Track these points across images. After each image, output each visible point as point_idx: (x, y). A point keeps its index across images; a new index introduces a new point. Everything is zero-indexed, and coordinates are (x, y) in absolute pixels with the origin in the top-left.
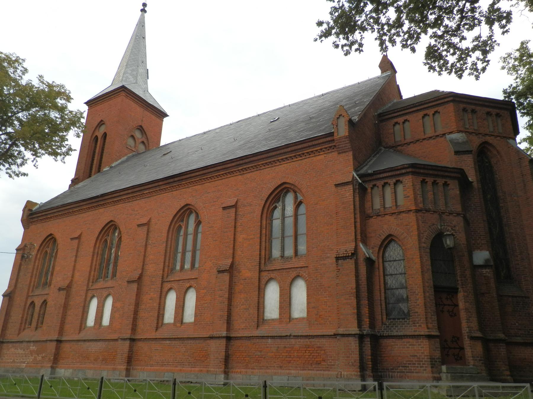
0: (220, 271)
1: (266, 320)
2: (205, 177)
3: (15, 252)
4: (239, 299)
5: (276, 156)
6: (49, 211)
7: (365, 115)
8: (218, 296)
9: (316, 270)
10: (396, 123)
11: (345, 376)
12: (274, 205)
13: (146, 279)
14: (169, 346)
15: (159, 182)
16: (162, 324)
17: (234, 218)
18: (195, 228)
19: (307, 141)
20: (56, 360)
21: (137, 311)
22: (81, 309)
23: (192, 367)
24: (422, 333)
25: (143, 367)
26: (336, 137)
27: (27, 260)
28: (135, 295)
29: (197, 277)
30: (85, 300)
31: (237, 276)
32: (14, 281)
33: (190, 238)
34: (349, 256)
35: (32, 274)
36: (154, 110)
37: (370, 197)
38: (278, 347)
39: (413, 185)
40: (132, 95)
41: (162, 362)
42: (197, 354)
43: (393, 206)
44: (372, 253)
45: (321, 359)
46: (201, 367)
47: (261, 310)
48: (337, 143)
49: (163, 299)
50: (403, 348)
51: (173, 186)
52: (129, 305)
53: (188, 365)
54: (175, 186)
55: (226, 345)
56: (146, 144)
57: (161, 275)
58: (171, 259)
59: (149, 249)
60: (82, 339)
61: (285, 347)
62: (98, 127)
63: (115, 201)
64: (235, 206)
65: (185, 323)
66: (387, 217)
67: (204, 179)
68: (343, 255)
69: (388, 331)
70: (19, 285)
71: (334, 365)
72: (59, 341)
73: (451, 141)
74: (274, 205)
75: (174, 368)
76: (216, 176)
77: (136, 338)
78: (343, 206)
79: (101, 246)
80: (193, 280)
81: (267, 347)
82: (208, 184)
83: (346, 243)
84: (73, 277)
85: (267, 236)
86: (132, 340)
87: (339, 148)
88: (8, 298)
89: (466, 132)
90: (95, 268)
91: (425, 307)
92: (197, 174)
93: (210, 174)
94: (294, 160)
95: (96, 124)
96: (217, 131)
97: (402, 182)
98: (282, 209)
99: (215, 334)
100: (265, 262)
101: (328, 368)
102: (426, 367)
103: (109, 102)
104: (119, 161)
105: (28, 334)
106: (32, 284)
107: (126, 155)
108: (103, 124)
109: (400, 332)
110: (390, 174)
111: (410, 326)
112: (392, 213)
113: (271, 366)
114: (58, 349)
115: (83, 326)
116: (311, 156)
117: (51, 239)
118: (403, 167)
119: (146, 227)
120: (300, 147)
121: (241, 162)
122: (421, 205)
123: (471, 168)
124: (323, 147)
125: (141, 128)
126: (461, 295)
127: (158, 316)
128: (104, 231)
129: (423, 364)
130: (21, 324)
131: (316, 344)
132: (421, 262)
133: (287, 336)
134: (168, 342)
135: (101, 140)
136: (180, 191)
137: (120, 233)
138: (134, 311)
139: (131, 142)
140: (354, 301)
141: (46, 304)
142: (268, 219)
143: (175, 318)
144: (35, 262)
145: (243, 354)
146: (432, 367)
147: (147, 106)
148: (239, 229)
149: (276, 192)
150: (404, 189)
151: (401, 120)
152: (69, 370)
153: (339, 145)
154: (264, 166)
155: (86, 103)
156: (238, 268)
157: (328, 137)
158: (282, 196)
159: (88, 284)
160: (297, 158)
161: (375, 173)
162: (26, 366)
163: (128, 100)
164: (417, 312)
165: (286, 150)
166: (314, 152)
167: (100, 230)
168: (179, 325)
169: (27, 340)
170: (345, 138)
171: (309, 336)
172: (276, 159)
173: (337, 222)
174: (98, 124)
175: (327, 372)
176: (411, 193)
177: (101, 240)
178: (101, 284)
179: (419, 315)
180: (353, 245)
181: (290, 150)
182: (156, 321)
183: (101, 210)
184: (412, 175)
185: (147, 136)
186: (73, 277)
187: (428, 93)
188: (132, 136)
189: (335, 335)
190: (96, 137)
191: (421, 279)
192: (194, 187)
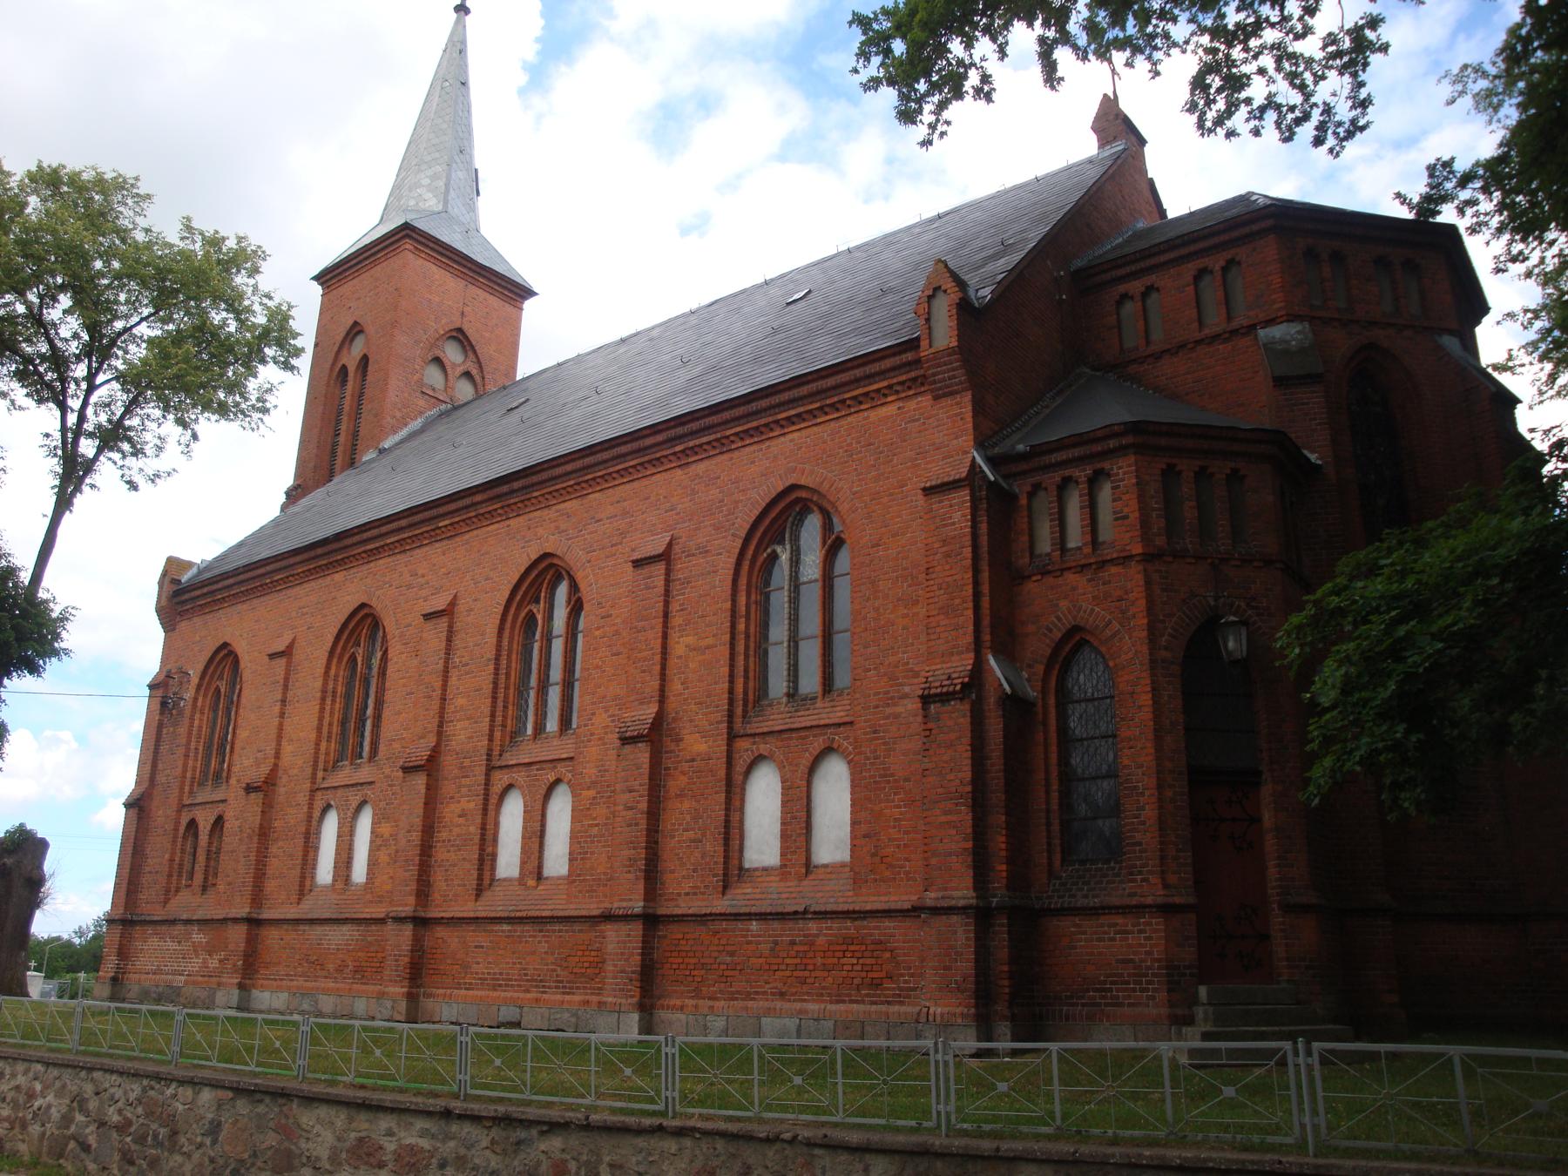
0: (626, 738)
1: (748, 870)
2: (590, 477)
3: (147, 692)
4: (678, 813)
5: (772, 411)
6: (217, 582)
7: (1016, 283)
8: (621, 807)
9: (875, 732)
10: (1125, 297)
11: (938, 1019)
12: (769, 550)
13: (448, 762)
14: (508, 937)
15: (473, 494)
16: (493, 880)
17: (661, 590)
18: (569, 618)
19: (849, 365)
20: (250, 967)
21: (431, 847)
22: (300, 841)
23: (564, 993)
24: (1149, 900)
25: (449, 991)
26: (925, 351)
27: (174, 712)
28: (422, 805)
29: (572, 755)
30: (310, 817)
31: (671, 752)
32: (148, 767)
33: (558, 646)
34: (954, 692)
35: (188, 749)
36: (495, 282)
37: (1026, 520)
38: (776, 943)
39: (1138, 484)
40: (431, 245)
41: (493, 979)
42: (577, 959)
43: (1085, 544)
44: (1028, 680)
45: (883, 974)
46: (586, 994)
47: (735, 843)
48: (929, 368)
49: (491, 813)
50: (1099, 940)
51: (509, 506)
52: (409, 831)
53: (556, 987)
54: (515, 503)
55: (644, 936)
56: (478, 378)
57: (484, 751)
58: (510, 707)
59: (453, 681)
60: (304, 917)
61: (793, 943)
62: (346, 346)
63: (371, 550)
64: (666, 557)
65: (547, 878)
66: (1070, 577)
67: (587, 481)
68: (939, 690)
69: (1063, 897)
70: (161, 778)
71: (914, 989)
72: (254, 922)
73: (1269, 347)
74: (769, 550)
75: (521, 995)
76: (618, 472)
77: (430, 915)
78: (944, 549)
79: (342, 673)
80: (563, 764)
81: (749, 943)
82: (597, 495)
83: (952, 654)
84: (277, 755)
85: (752, 639)
86: (421, 923)
87: (935, 382)
88: (136, 810)
89: (1314, 318)
90: (330, 733)
91: (1160, 829)
92: (569, 467)
93: (601, 467)
94: (819, 420)
95: (343, 334)
96: (655, 333)
97: (1109, 475)
98: (791, 559)
99: (617, 906)
100: (745, 712)
101: (900, 996)
102: (1155, 990)
103: (372, 271)
104: (404, 433)
105: (186, 903)
106: (189, 775)
107: (421, 413)
108: (361, 331)
109: (1094, 897)
110: (1077, 452)
111: (1120, 882)
112: (1083, 566)
113: (757, 993)
114: (252, 941)
115: (308, 883)
116: (862, 407)
117: (225, 659)
118: (1110, 432)
119: (445, 619)
120: (831, 382)
121: (680, 430)
122: (1160, 541)
123: (1320, 424)
124: (895, 381)
125: (459, 336)
126: (1267, 791)
127: (481, 860)
128: (345, 637)
129: (1149, 983)
130: (170, 875)
131: (871, 935)
132: (1155, 702)
133: (796, 913)
134: (505, 927)
135: (355, 377)
136: (526, 517)
137: (574, 587)
138: (422, 845)
139: (434, 376)
140: (965, 816)
141: (222, 827)
142: (753, 590)
143: (523, 863)
144: (192, 719)
145: (687, 960)
146: (1169, 991)
147: (474, 271)
148: (677, 620)
149: (772, 515)
150: (1113, 494)
151: (1136, 287)
152: (280, 995)
153: (934, 375)
154: (742, 439)
155: (317, 278)
156: (674, 729)
157: (905, 351)
158: (789, 525)
159: (314, 775)
160: (826, 414)
161: (1036, 452)
162: (186, 982)
163: (420, 262)
164: (1140, 844)
165: (795, 393)
166: (872, 395)
167: (336, 631)
168: (531, 883)
169: (184, 917)
170: (949, 355)
171: (854, 912)
172: (771, 419)
173: (928, 595)
174: (348, 334)
175: (896, 1008)
176: (1132, 509)
177: (207, 689)
178: (345, 775)
179: (1145, 851)
180: (965, 662)
181: (805, 393)
182: (475, 874)
183: (338, 577)
184: (1135, 453)
185: (477, 357)
186: (277, 755)
187: (1227, 202)
188: (438, 361)
189: (915, 911)
190: (344, 368)
191: (1153, 751)
192: (562, 506)
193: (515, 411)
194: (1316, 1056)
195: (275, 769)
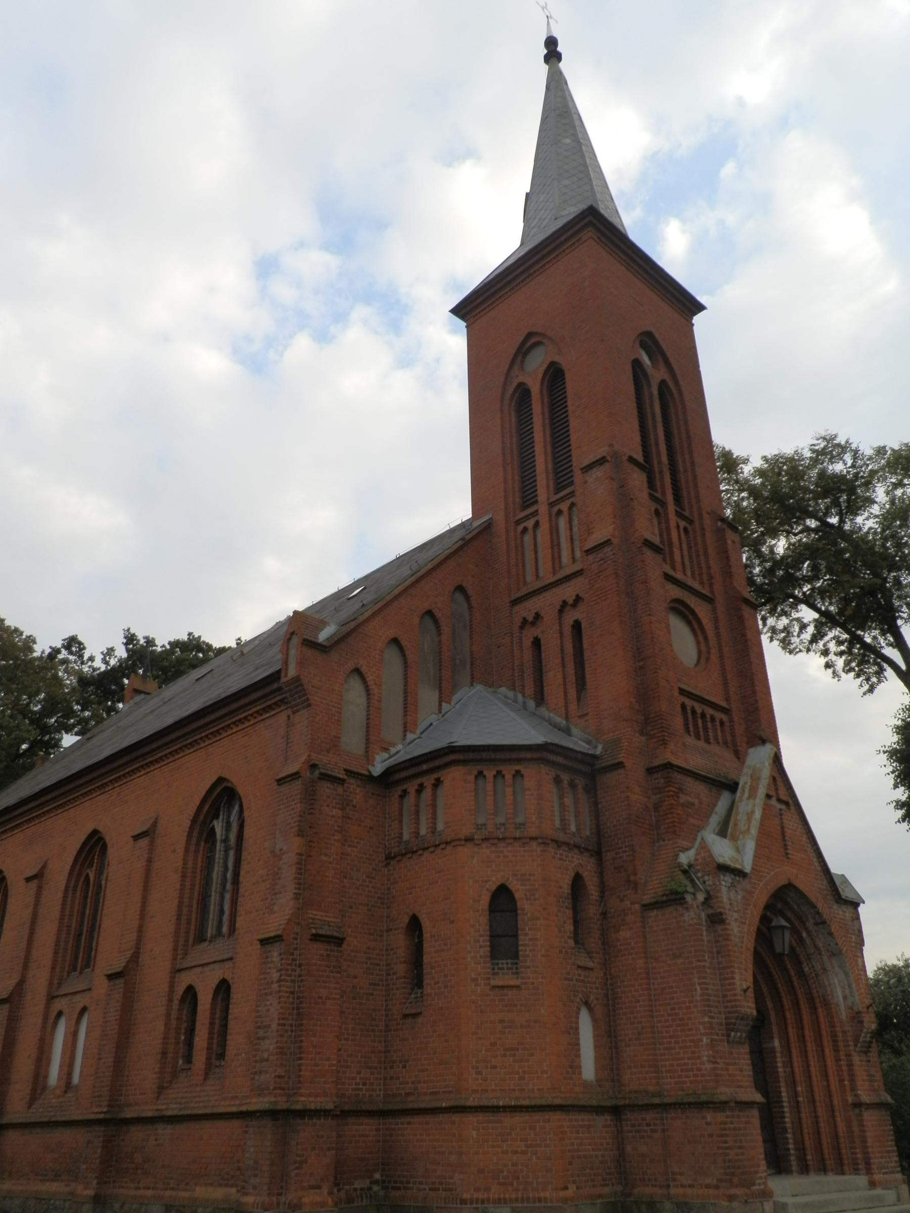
190: (523, 393)
193: (203, 680)
195: (135, 957)
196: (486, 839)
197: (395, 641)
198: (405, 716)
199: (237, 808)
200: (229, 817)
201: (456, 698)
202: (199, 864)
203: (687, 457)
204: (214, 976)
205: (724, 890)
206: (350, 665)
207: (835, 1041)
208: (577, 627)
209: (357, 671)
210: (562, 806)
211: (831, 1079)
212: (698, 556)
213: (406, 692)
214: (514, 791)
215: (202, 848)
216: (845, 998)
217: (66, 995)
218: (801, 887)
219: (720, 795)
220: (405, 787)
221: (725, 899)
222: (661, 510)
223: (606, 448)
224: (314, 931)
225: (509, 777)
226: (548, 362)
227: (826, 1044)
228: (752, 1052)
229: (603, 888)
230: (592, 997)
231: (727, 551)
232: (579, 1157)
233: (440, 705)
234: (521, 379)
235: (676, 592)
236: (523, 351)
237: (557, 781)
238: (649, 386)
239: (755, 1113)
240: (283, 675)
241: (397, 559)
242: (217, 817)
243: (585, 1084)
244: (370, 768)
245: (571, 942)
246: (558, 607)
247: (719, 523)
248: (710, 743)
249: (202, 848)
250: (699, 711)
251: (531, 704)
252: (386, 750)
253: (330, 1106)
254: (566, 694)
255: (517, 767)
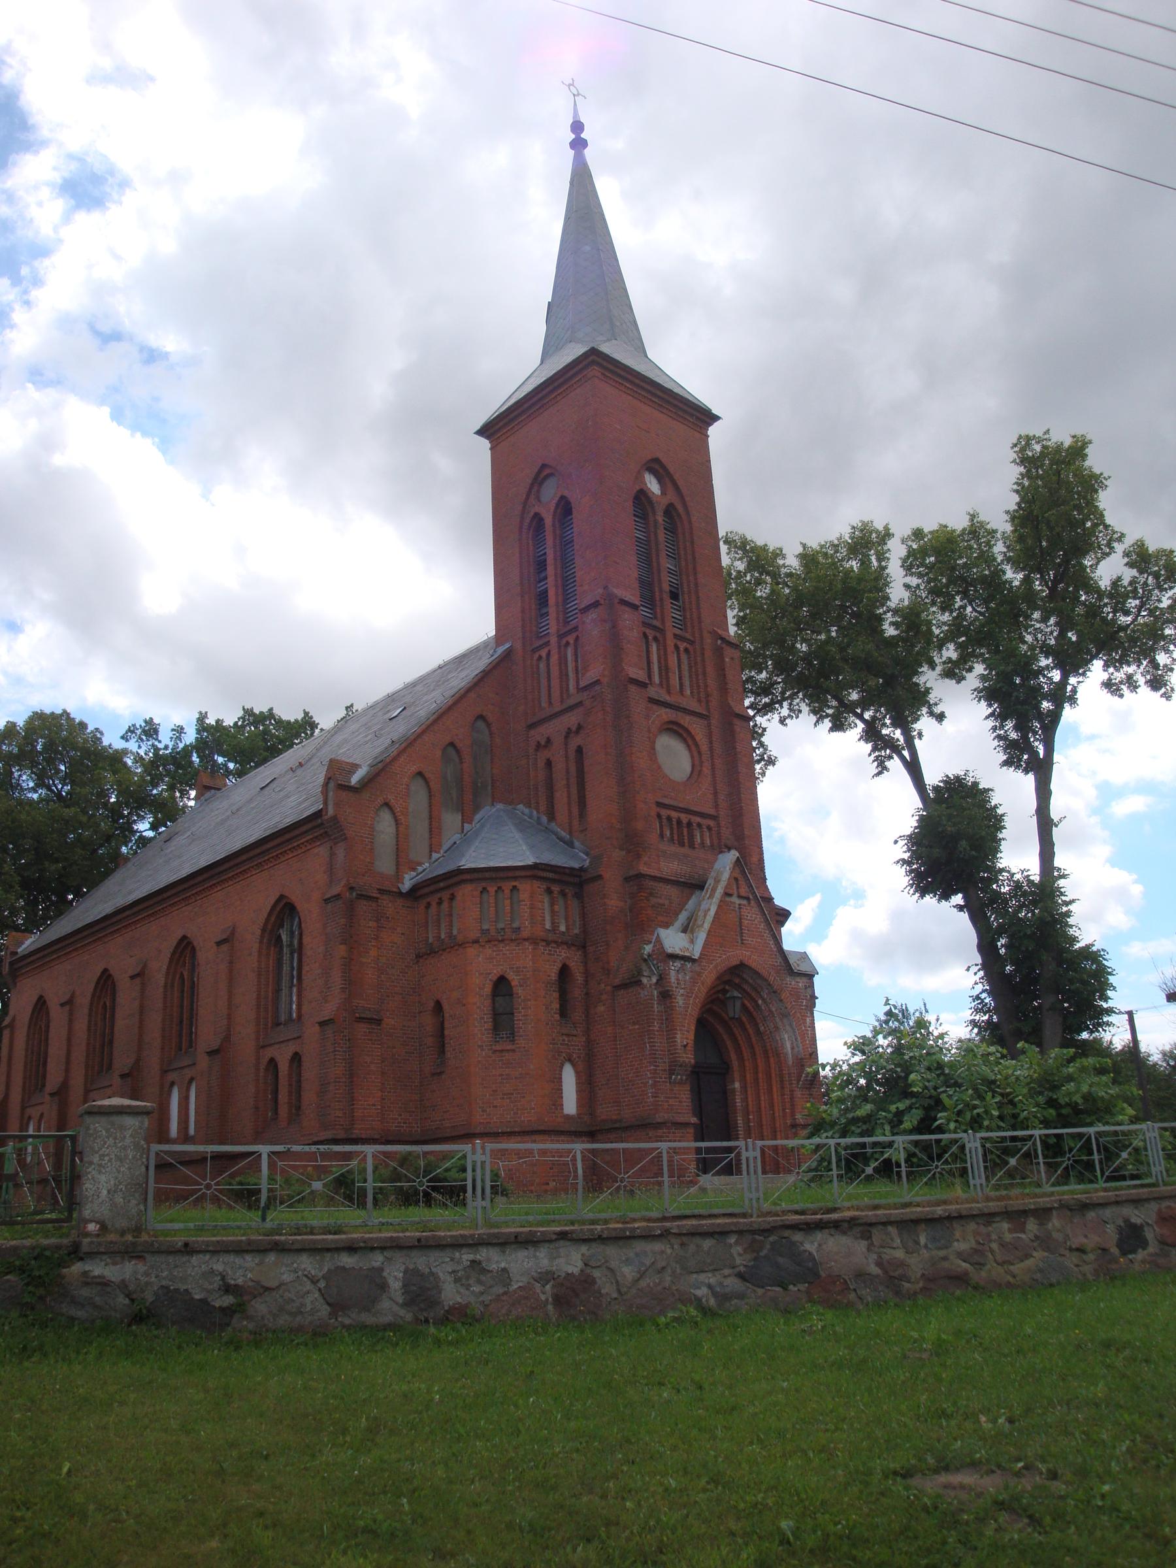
141: (300, 1060)
155: (484, 431)
190: (538, 519)
193: (267, 789)
194: (758, 1150)
195: (227, 1038)
196: (489, 941)
197: (420, 774)
198: (431, 838)
199: (297, 919)
200: (292, 926)
201: (478, 817)
202: (271, 964)
203: (691, 578)
204: (290, 1049)
205: (673, 973)
206: (380, 801)
207: (782, 1081)
208: (579, 750)
209: (387, 804)
210: (553, 912)
211: (776, 1109)
212: (697, 675)
213: (431, 818)
214: (512, 904)
215: (272, 952)
216: (793, 1048)
217: (176, 1069)
218: (753, 965)
219: (692, 895)
220: (428, 900)
221: (673, 980)
222: (658, 635)
223: (601, 591)
224: (357, 1015)
225: (507, 892)
226: (559, 496)
227: (774, 1082)
228: (692, 1091)
229: (587, 974)
230: (574, 1056)
231: (724, 669)
232: (558, 1165)
233: (463, 826)
234: (537, 509)
235: (665, 714)
236: (539, 480)
237: (549, 891)
238: (654, 513)
239: (692, 1130)
240: (324, 813)
241: (440, 667)
242: (282, 926)
243: (568, 1117)
244: (400, 885)
245: (557, 1017)
246: (564, 734)
247: (719, 642)
248: (694, 848)
249: (272, 952)
250: (685, 821)
251: (544, 819)
252: (414, 869)
253: (376, 1137)
254: (570, 810)
255: (514, 884)
